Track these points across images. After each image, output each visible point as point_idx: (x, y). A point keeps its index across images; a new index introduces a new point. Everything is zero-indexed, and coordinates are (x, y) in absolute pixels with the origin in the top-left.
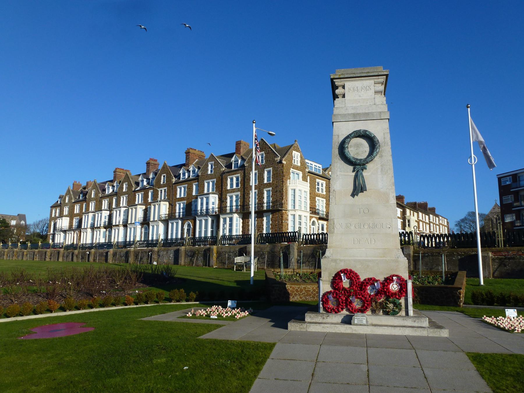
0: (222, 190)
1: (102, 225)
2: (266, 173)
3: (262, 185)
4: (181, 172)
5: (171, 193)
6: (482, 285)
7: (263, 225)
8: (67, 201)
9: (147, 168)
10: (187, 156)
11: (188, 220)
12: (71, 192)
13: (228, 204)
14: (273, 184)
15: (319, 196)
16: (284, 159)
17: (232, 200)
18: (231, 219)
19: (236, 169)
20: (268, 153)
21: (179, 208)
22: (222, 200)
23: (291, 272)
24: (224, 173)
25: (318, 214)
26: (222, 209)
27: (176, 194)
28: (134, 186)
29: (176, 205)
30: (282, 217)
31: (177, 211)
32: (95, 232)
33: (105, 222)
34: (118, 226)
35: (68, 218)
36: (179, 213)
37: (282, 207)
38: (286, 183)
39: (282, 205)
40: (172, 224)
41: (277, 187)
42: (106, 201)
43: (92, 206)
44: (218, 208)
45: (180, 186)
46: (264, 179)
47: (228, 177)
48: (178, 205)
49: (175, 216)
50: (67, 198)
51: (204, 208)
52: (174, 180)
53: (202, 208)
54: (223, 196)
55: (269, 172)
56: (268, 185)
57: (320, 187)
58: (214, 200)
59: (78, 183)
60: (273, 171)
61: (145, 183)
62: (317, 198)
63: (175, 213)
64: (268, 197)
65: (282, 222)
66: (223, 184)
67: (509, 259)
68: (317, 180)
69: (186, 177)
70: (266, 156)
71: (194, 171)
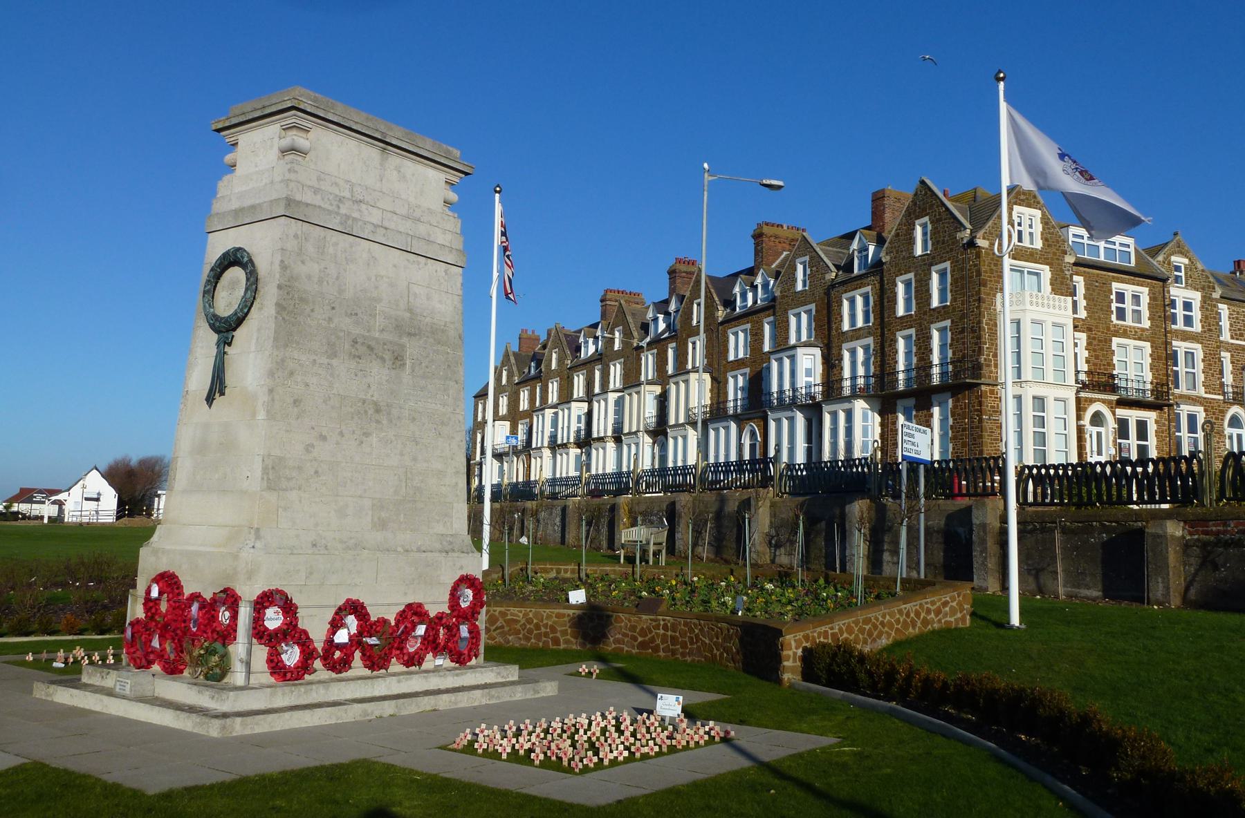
0: (829, 335)
1: (572, 440)
2: (935, 278)
3: (925, 313)
4: (737, 290)
5: (716, 350)
6: (1012, 628)
9: (671, 284)
10: (757, 245)
11: (750, 419)
12: (512, 359)
13: (847, 373)
14: (954, 309)
15: (1125, 333)
16: (980, 234)
17: (855, 364)
18: (849, 415)
19: (863, 271)
20: (939, 220)
21: (735, 386)
22: (831, 363)
23: (573, 571)
24: (833, 285)
25: (1113, 389)
27: (727, 351)
28: (635, 334)
29: (726, 382)
30: (980, 404)
31: (731, 397)
32: (559, 457)
33: (579, 431)
34: (601, 439)
35: (508, 423)
36: (736, 400)
37: (979, 376)
38: (993, 303)
39: (977, 369)
40: (717, 430)
41: (963, 317)
42: (618, 366)
43: (553, 388)
45: (734, 330)
48: (731, 381)
49: (725, 409)
50: (505, 373)
51: (787, 386)
52: (721, 313)
53: (781, 384)
54: (834, 351)
55: (942, 274)
56: (941, 313)
57: (1128, 306)
58: (808, 366)
59: (530, 333)
60: (953, 271)
61: (662, 326)
62: (1115, 340)
63: (726, 401)
64: (943, 347)
65: (981, 420)
66: (833, 319)
67: (1227, 544)
68: (1116, 286)
69: (750, 303)
70: (934, 229)
71: (765, 285)
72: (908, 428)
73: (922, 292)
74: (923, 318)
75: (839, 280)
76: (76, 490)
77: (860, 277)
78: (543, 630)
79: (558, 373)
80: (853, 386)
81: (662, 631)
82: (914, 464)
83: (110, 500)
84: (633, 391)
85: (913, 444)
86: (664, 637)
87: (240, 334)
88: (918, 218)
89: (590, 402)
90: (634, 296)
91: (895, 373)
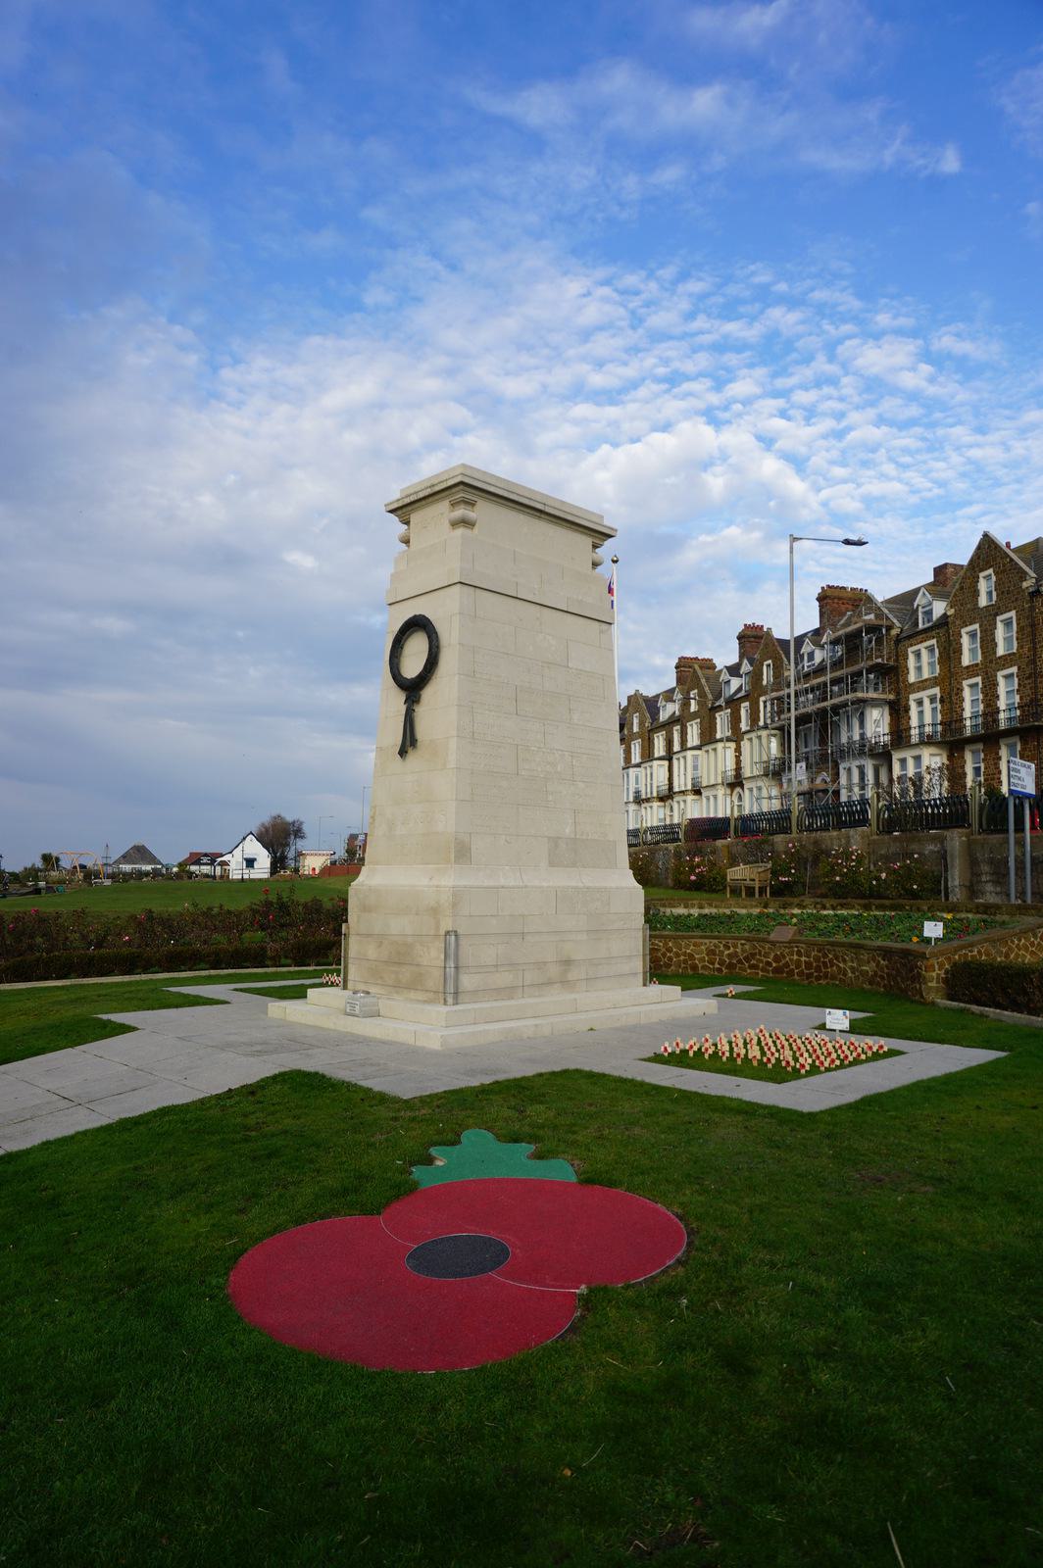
7: (1000, 772)
8: (636, 729)
13: (914, 722)
19: (927, 625)
20: (1004, 571)
26: (900, 735)
42: (695, 726)
44: (891, 733)
46: (996, 645)
47: (910, 650)
56: (1007, 660)
60: (1018, 620)
72: (1015, 763)
73: (988, 643)
74: (989, 666)
75: (904, 635)
76: (238, 852)
77: (925, 631)
78: (682, 958)
79: (640, 735)
80: (921, 734)
81: (795, 957)
82: (1020, 797)
83: (264, 860)
84: (709, 748)
85: (1019, 779)
86: (798, 964)
87: (428, 694)
88: (982, 570)
89: (670, 760)
90: (708, 665)
91: (961, 720)
